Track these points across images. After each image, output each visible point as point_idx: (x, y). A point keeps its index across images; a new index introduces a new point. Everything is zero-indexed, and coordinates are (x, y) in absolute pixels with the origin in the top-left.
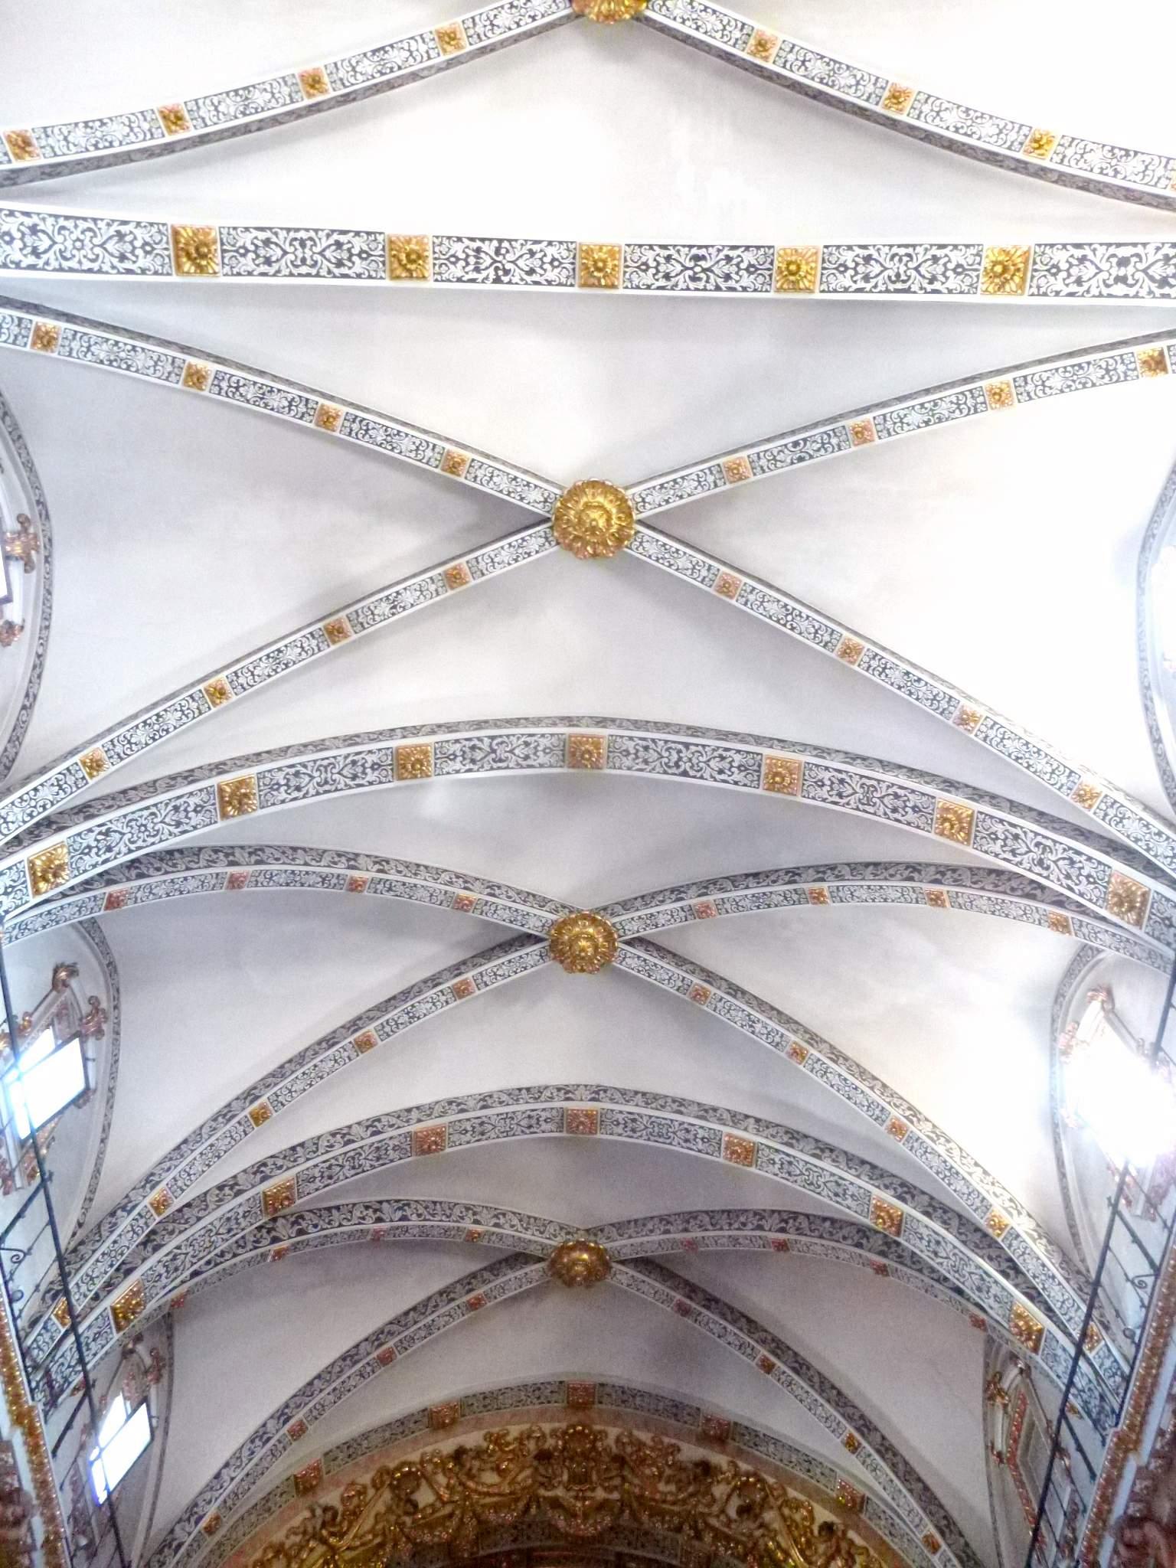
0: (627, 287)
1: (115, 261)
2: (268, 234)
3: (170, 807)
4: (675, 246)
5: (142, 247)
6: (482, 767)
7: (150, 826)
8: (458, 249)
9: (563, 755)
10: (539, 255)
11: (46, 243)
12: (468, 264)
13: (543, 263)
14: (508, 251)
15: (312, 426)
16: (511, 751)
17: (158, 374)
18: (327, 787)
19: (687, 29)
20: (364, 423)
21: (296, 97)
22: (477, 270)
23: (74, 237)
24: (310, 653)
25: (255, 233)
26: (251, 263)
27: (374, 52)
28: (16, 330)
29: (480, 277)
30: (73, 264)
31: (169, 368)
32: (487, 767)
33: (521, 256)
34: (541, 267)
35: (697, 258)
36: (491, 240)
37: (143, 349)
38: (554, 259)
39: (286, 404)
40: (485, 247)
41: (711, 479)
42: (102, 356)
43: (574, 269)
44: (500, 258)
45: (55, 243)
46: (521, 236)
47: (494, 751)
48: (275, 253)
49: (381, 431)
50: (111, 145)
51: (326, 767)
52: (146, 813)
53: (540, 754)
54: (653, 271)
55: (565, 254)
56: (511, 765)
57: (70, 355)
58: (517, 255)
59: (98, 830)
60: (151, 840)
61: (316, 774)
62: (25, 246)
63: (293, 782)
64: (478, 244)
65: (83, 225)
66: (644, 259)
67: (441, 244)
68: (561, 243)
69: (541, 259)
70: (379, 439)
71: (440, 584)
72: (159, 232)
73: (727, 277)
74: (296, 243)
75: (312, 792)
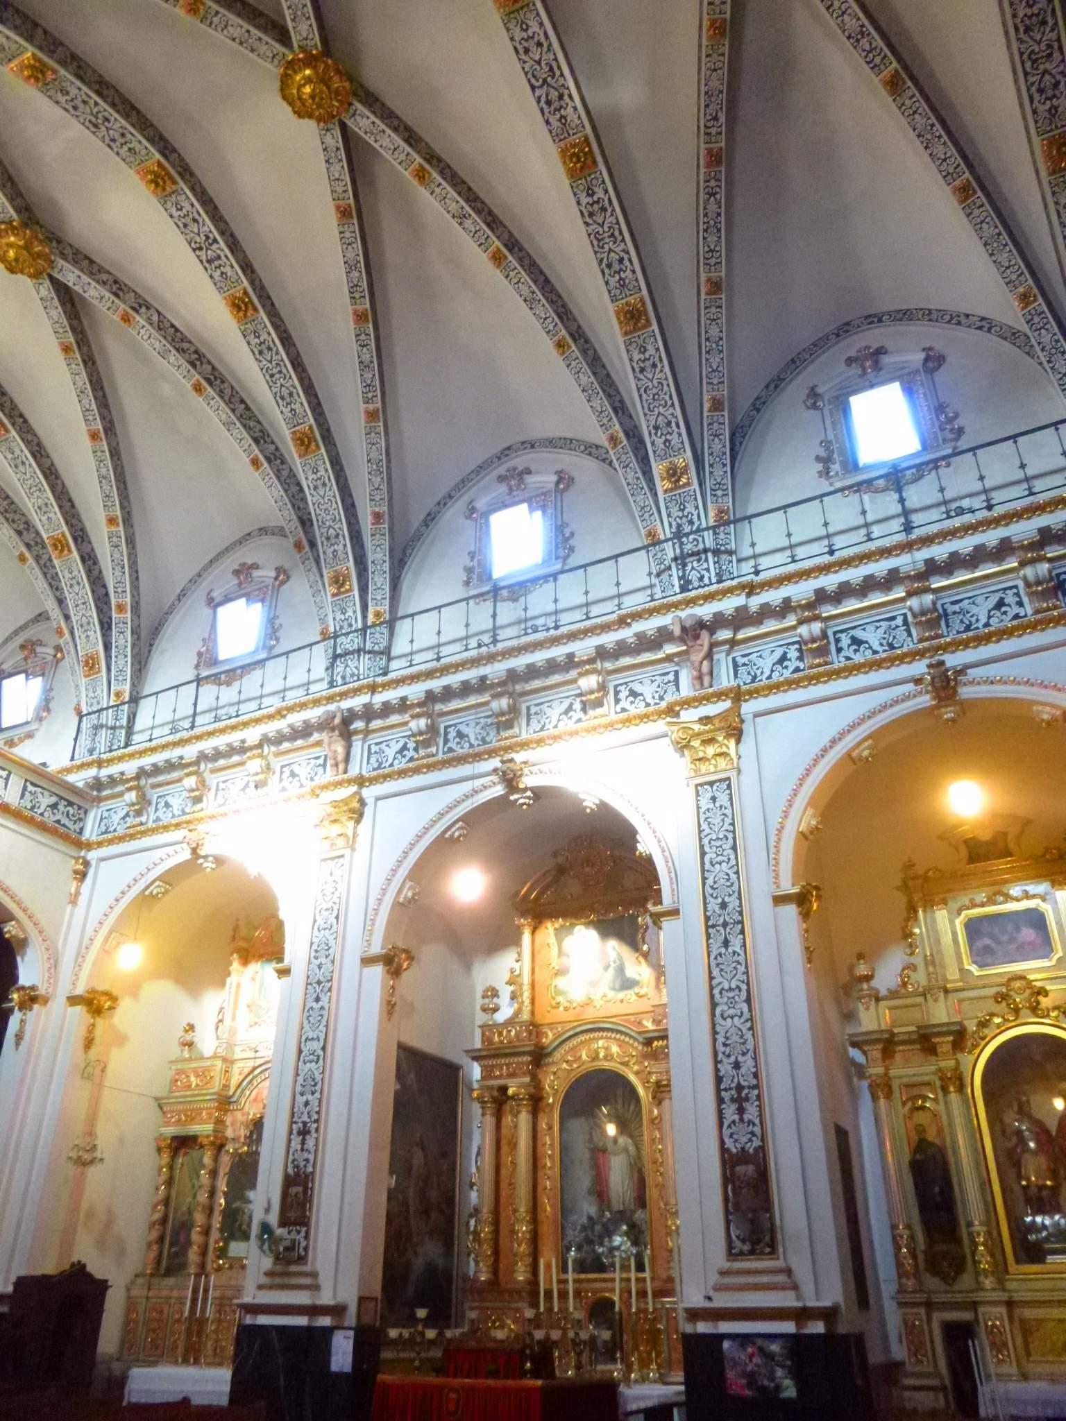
3: (641, 376)
6: (563, 85)
7: (655, 391)
9: (522, 8)
16: (539, 62)
18: (617, 233)
30: (667, 397)
32: (561, 81)
35: (96, 126)
41: (216, 20)
46: (182, 238)
47: (545, 81)
48: (285, 392)
51: (599, 241)
52: (644, 397)
53: (530, 32)
56: (552, 57)
59: (654, 437)
60: (665, 388)
61: (606, 247)
63: (616, 267)
70: (357, 274)
73: (85, 102)
75: (622, 246)
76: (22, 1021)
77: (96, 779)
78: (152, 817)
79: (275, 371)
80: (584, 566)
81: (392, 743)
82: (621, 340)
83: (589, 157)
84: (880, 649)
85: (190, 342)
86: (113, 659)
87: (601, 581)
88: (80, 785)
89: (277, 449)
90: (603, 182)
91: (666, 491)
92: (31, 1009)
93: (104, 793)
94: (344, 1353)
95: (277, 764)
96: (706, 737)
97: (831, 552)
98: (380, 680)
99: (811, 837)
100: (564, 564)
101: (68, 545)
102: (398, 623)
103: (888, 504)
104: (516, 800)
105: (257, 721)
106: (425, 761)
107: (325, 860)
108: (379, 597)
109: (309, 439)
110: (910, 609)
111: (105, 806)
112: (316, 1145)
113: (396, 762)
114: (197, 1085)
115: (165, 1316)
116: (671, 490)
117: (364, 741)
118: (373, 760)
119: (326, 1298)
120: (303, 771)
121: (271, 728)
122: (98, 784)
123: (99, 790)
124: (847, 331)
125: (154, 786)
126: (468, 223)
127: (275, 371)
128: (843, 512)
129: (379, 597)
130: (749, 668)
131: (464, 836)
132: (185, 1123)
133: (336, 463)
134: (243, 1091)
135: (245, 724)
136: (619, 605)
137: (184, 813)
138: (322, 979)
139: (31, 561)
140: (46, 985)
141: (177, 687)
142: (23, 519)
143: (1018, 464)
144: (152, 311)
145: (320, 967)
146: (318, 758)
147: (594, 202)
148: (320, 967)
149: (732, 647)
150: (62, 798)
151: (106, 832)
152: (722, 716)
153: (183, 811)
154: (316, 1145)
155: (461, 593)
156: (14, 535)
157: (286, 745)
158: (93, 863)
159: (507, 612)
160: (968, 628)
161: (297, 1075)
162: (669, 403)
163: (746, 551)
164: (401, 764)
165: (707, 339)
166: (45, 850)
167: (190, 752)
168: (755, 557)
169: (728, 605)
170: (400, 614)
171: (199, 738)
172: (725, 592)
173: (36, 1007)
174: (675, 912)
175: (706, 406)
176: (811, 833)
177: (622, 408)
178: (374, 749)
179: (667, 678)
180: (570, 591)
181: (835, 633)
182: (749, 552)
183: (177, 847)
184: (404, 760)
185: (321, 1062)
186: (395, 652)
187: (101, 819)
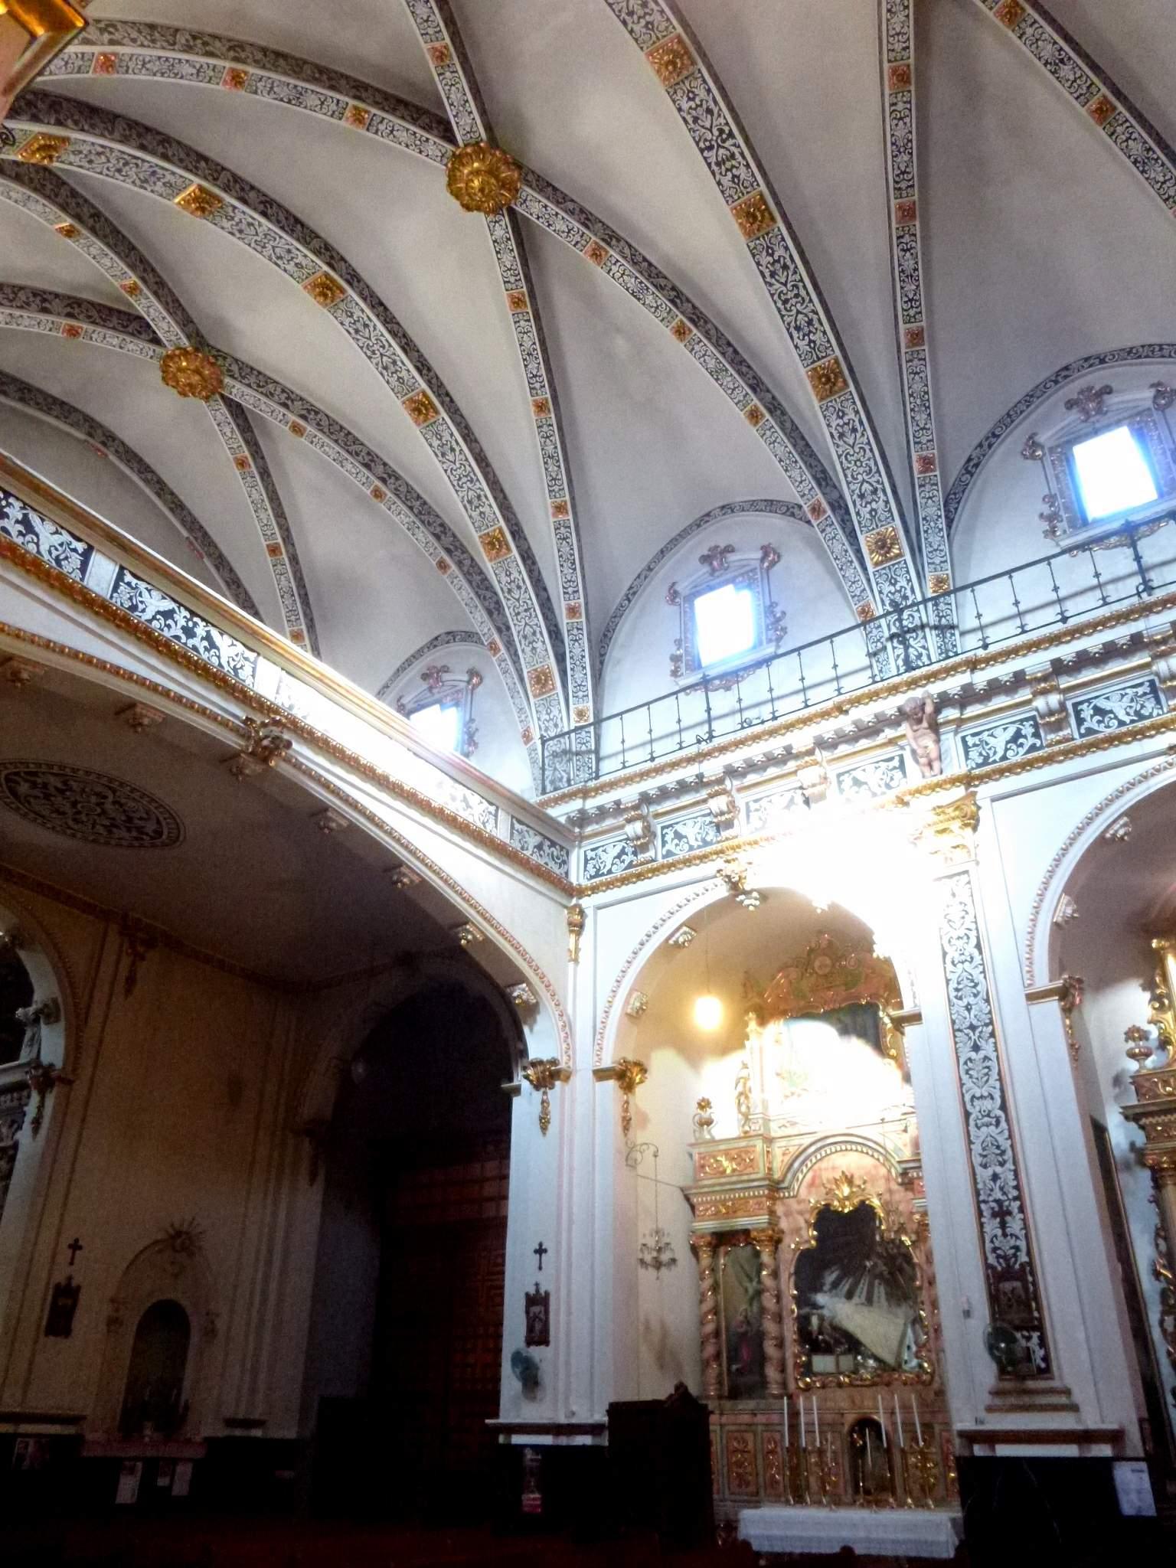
0: (674, 28)
1: (858, 435)
2: (792, 330)
4: (618, 16)
5: (842, 418)
8: (726, 181)
10: (694, 113)
11: (866, 485)
12: (733, 166)
13: (697, 106)
14: (706, 140)
15: (917, 223)
17: (923, 368)
19: (472, 105)
20: (897, 179)
21: (697, 340)
22: (733, 156)
23: (855, 468)
24: (1131, 130)
25: (796, 340)
26: (817, 335)
27: (639, 299)
28: (928, 486)
29: (736, 151)
30: (872, 463)
31: (916, 362)
33: (703, 127)
34: (701, 105)
36: (705, 159)
37: (909, 388)
38: (690, 99)
39: (908, 254)
40: (713, 160)
42: (924, 416)
43: (686, 78)
44: (713, 143)
45: (864, 480)
49: (899, 160)
50: (790, 453)
54: (647, 17)
55: (680, 93)
57: (932, 440)
58: (703, 130)
62: (874, 500)
64: (714, 167)
65: (846, 464)
66: (644, 30)
67: (731, 196)
68: (674, 101)
69: (695, 109)
70: (906, 158)
71: (1023, 25)
72: (827, 409)
74: (788, 306)
76: (543, 1102)
77: (582, 811)
78: (661, 852)
79: (790, 295)
80: (798, 650)
81: (998, 732)
82: (816, 404)
83: (766, 214)
84: (1127, 719)
85: (665, 278)
86: (569, 673)
87: (818, 665)
88: (563, 820)
89: (774, 398)
90: (783, 239)
91: (877, 564)
92: (552, 1087)
93: (589, 830)
94: (1139, 1492)
95: (741, 800)
96: (941, 827)
97: (1064, 620)
98: (592, 784)
99: (1066, 926)
100: (778, 647)
101: (507, 545)
102: (605, 724)
103: (1119, 561)
104: (742, 902)
105: (806, 721)
106: (1062, 746)
107: (940, 879)
108: (937, 560)
109: (836, 377)
110: (1157, 674)
111: (587, 845)
112: (1026, 1227)
113: (1010, 754)
114: (734, 1170)
115: (750, 1446)
116: (882, 562)
117: (956, 732)
118: (590, 866)
119: (1091, 1420)
120: (873, 777)
121: (827, 728)
122: (582, 819)
123: (581, 827)
124: (1066, 377)
125: (657, 815)
126: (1066, 71)
127: (790, 295)
128: (1077, 572)
129: (937, 560)
130: (980, 749)
131: (690, 941)
132: (727, 1215)
133: (528, 557)
134: (795, 1174)
135: (789, 727)
136: (839, 690)
137: (706, 843)
138: (975, 1022)
139: (454, 567)
140: (565, 1058)
141: (648, 704)
142: (439, 521)
143: (1093, 573)
144: (622, 243)
145: (968, 1008)
146: (891, 759)
147: (775, 261)
148: (968, 1008)
149: (959, 726)
150: (546, 837)
151: (597, 875)
152: (957, 805)
153: (704, 840)
154: (1026, 1227)
155: (669, 685)
156: (431, 538)
157: (844, 749)
158: (589, 912)
159: (722, 701)
160: (985, 763)
161: (970, 1142)
162: (874, 469)
163: (971, 622)
164: (1016, 756)
165: (911, 395)
166: (540, 898)
167: (712, 768)
168: (981, 628)
169: (953, 684)
170: (605, 715)
171: (723, 749)
172: (949, 671)
173: (558, 1083)
174: (916, 1018)
175: (916, 466)
176: (1067, 922)
177: (825, 479)
178: (970, 741)
179: (892, 764)
180: (784, 674)
181: (1075, 705)
182: (975, 623)
183: (709, 884)
184: (1022, 751)
185: (1003, 1124)
186: (603, 752)
187: (586, 861)
